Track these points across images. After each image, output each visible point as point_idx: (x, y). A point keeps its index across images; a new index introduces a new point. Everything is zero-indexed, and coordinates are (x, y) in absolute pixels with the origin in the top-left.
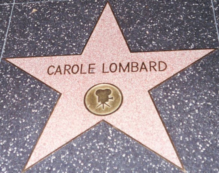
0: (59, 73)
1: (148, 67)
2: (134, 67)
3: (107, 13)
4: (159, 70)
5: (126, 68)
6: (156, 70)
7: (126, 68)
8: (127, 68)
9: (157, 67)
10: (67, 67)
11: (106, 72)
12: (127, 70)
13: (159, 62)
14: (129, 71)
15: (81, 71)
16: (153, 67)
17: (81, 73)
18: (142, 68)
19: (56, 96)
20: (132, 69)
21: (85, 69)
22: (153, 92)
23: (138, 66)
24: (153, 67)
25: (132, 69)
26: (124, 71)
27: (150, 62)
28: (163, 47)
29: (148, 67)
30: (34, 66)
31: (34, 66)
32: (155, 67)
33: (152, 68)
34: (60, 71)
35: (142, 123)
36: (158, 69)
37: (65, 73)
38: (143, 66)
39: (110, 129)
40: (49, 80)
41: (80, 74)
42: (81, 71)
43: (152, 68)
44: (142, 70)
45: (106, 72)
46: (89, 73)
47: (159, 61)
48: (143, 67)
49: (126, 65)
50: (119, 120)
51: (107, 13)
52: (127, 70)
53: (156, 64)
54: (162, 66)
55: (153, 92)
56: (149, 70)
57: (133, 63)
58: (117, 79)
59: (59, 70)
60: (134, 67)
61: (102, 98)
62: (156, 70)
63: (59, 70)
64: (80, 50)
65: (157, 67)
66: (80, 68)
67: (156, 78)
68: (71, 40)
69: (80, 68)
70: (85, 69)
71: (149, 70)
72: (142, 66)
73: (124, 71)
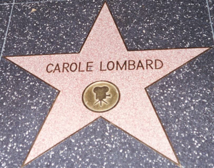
1: (145, 65)
2: (131, 65)
3: (105, 12)
4: (156, 68)
5: (123, 66)
6: (152, 68)
7: (123, 66)
10: (66, 65)
11: (89, 71)
12: (124, 68)
13: (156, 60)
14: (126, 69)
16: (150, 65)
18: (138, 66)
21: (84, 67)
22: (149, 90)
23: (135, 65)
24: (150, 65)
26: (121, 69)
27: (147, 61)
29: (145, 65)
30: (33, 64)
31: (33, 64)
32: (151, 65)
33: (148, 66)
34: (59, 69)
36: (154, 67)
38: (140, 64)
39: (107, 125)
41: (78, 72)
43: (148, 66)
48: (140, 65)
49: (123, 63)
50: (117, 117)
52: (124, 68)
54: (159, 64)
55: (149, 90)
56: (145, 68)
57: (130, 62)
59: (57, 68)
60: (131, 65)
61: (100, 95)
62: (152, 68)
63: (57, 68)
64: (78, 48)
65: (153, 66)
66: (78, 66)
67: (152, 76)
68: (69, 38)
69: (78, 66)
71: (145, 68)
72: (139, 64)
73: (121, 69)
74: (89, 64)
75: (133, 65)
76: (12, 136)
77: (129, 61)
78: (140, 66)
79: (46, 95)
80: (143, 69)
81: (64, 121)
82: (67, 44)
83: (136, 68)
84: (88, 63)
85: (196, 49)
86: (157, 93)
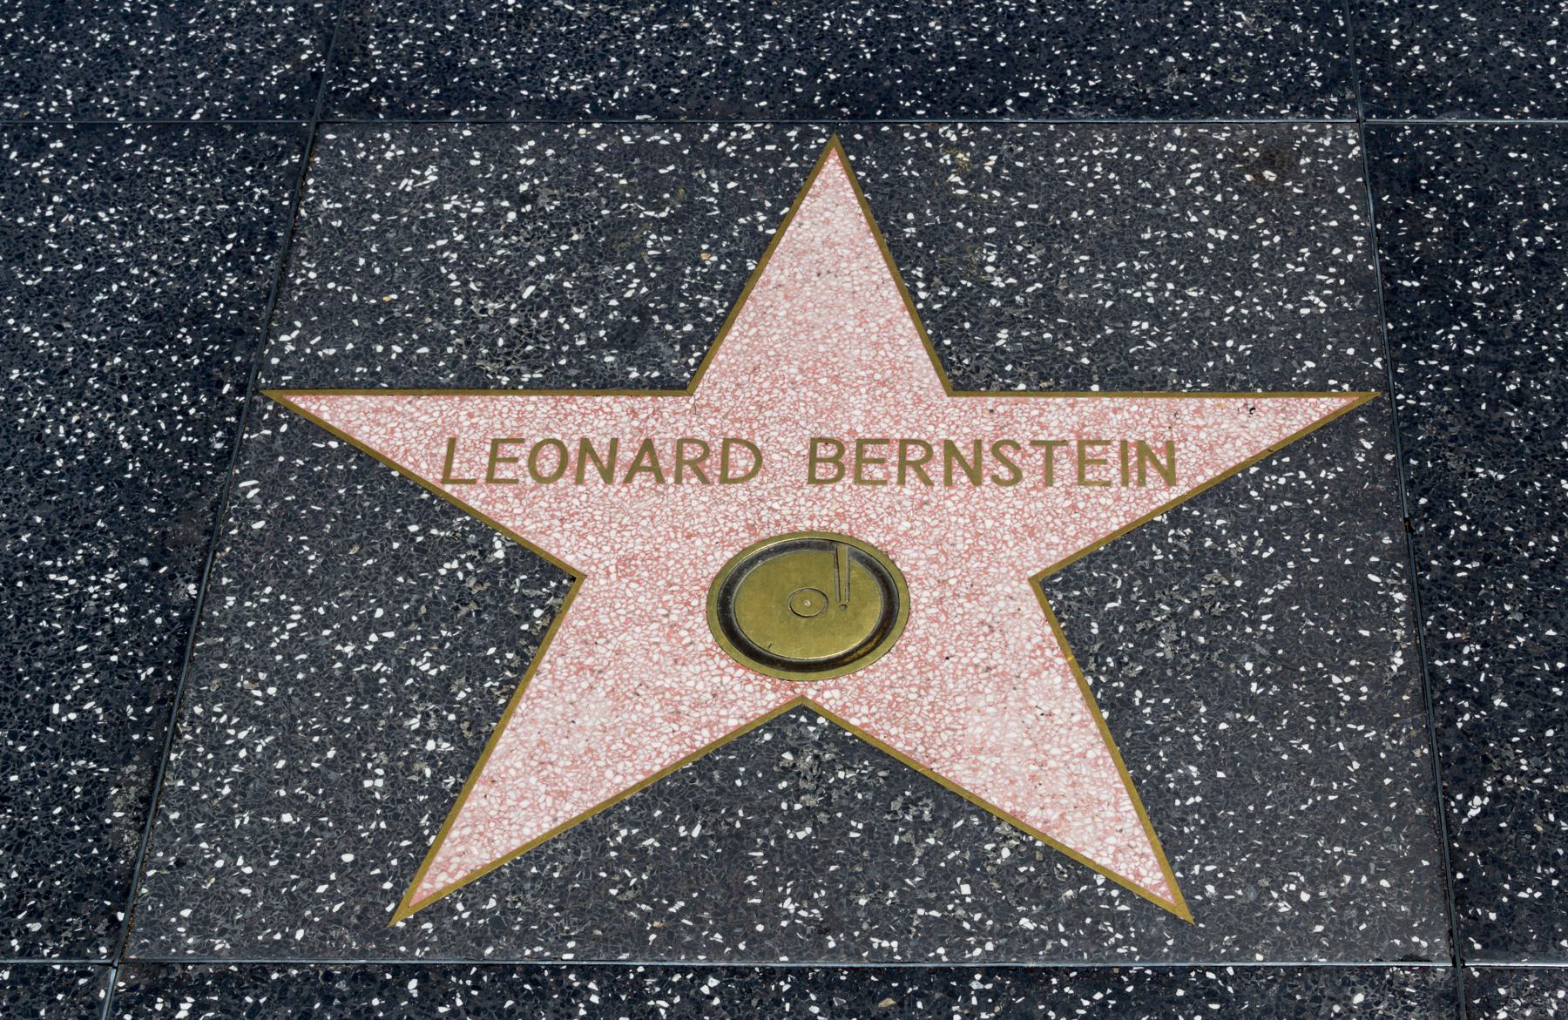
2: (821, 460)
3: (833, 171)
4: (724, 479)
9: (712, 466)
10: (916, 454)
11: (498, 481)
13: (727, 443)
19: (552, 579)
22: (1071, 592)
23: (842, 461)
28: (328, 448)
29: (667, 461)
33: (687, 469)
35: (1013, 733)
43: (911, 473)
45: (498, 481)
46: (812, 479)
51: (833, 171)
53: (707, 452)
54: (741, 461)
55: (1071, 592)
58: (879, 514)
59: (645, 462)
60: (821, 460)
62: (929, 483)
65: (712, 466)
67: (1113, 509)
71: (619, 476)
75: (835, 460)
76: (217, 709)
79: (516, 601)
81: (573, 745)
82: (1273, 236)
84: (496, 443)
85: (424, 401)
86: (1093, 602)
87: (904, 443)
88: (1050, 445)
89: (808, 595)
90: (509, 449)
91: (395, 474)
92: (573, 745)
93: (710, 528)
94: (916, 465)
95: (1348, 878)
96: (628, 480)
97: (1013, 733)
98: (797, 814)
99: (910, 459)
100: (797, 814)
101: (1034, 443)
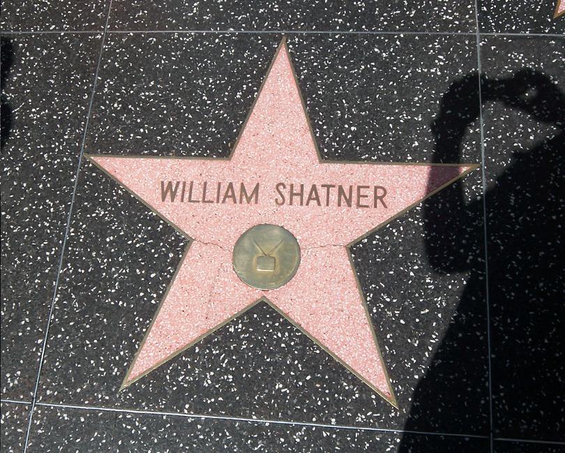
0: (316, 201)
4: (190, 201)
5: (252, 195)
8: (254, 195)
10: (380, 193)
11: (194, 202)
15: (302, 199)
17: (190, 201)
20: (358, 201)
21: (197, 193)
25: (358, 201)
26: (249, 200)
33: (378, 200)
34: (233, 196)
35: (336, 317)
37: (241, 202)
39: (436, 364)
40: (169, 211)
42: (302, 199)
43: (378, 200)
44: (311, 201)
45: (194, 202)
47: (375, 185)
50: (292, 302)
56: (238, 201)
57: (361, 189)
58: (295, 218)
59: (230, 194)
63: (230, 194)
67: (365, 221)
70: (197, 193)
73: (249, 200)
74: (363, 191)
77: (359, 188)
78: (314, 199)
79: (161, 248)
80: (235, 202)
81: (194, 306)
83: (288, 200)
86: (369, 258)
87: (376, 188)
88: (328, 187)
89: (274, 253)
90: (363, 191)
91: (132, 196)
92: (194, 306)
93: (247, 216)
94: (381, 198)
95: (189, 367)
96: (307, 204)
97: (336, 317)
98: (261, 345)
99: (378, 195)
100: (261, 345)
101: (323, 186)
